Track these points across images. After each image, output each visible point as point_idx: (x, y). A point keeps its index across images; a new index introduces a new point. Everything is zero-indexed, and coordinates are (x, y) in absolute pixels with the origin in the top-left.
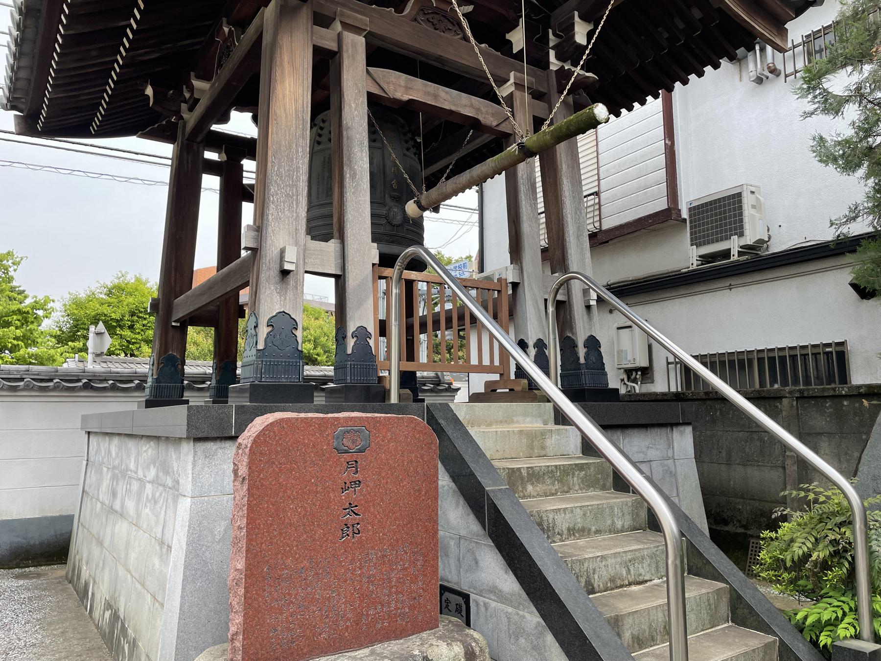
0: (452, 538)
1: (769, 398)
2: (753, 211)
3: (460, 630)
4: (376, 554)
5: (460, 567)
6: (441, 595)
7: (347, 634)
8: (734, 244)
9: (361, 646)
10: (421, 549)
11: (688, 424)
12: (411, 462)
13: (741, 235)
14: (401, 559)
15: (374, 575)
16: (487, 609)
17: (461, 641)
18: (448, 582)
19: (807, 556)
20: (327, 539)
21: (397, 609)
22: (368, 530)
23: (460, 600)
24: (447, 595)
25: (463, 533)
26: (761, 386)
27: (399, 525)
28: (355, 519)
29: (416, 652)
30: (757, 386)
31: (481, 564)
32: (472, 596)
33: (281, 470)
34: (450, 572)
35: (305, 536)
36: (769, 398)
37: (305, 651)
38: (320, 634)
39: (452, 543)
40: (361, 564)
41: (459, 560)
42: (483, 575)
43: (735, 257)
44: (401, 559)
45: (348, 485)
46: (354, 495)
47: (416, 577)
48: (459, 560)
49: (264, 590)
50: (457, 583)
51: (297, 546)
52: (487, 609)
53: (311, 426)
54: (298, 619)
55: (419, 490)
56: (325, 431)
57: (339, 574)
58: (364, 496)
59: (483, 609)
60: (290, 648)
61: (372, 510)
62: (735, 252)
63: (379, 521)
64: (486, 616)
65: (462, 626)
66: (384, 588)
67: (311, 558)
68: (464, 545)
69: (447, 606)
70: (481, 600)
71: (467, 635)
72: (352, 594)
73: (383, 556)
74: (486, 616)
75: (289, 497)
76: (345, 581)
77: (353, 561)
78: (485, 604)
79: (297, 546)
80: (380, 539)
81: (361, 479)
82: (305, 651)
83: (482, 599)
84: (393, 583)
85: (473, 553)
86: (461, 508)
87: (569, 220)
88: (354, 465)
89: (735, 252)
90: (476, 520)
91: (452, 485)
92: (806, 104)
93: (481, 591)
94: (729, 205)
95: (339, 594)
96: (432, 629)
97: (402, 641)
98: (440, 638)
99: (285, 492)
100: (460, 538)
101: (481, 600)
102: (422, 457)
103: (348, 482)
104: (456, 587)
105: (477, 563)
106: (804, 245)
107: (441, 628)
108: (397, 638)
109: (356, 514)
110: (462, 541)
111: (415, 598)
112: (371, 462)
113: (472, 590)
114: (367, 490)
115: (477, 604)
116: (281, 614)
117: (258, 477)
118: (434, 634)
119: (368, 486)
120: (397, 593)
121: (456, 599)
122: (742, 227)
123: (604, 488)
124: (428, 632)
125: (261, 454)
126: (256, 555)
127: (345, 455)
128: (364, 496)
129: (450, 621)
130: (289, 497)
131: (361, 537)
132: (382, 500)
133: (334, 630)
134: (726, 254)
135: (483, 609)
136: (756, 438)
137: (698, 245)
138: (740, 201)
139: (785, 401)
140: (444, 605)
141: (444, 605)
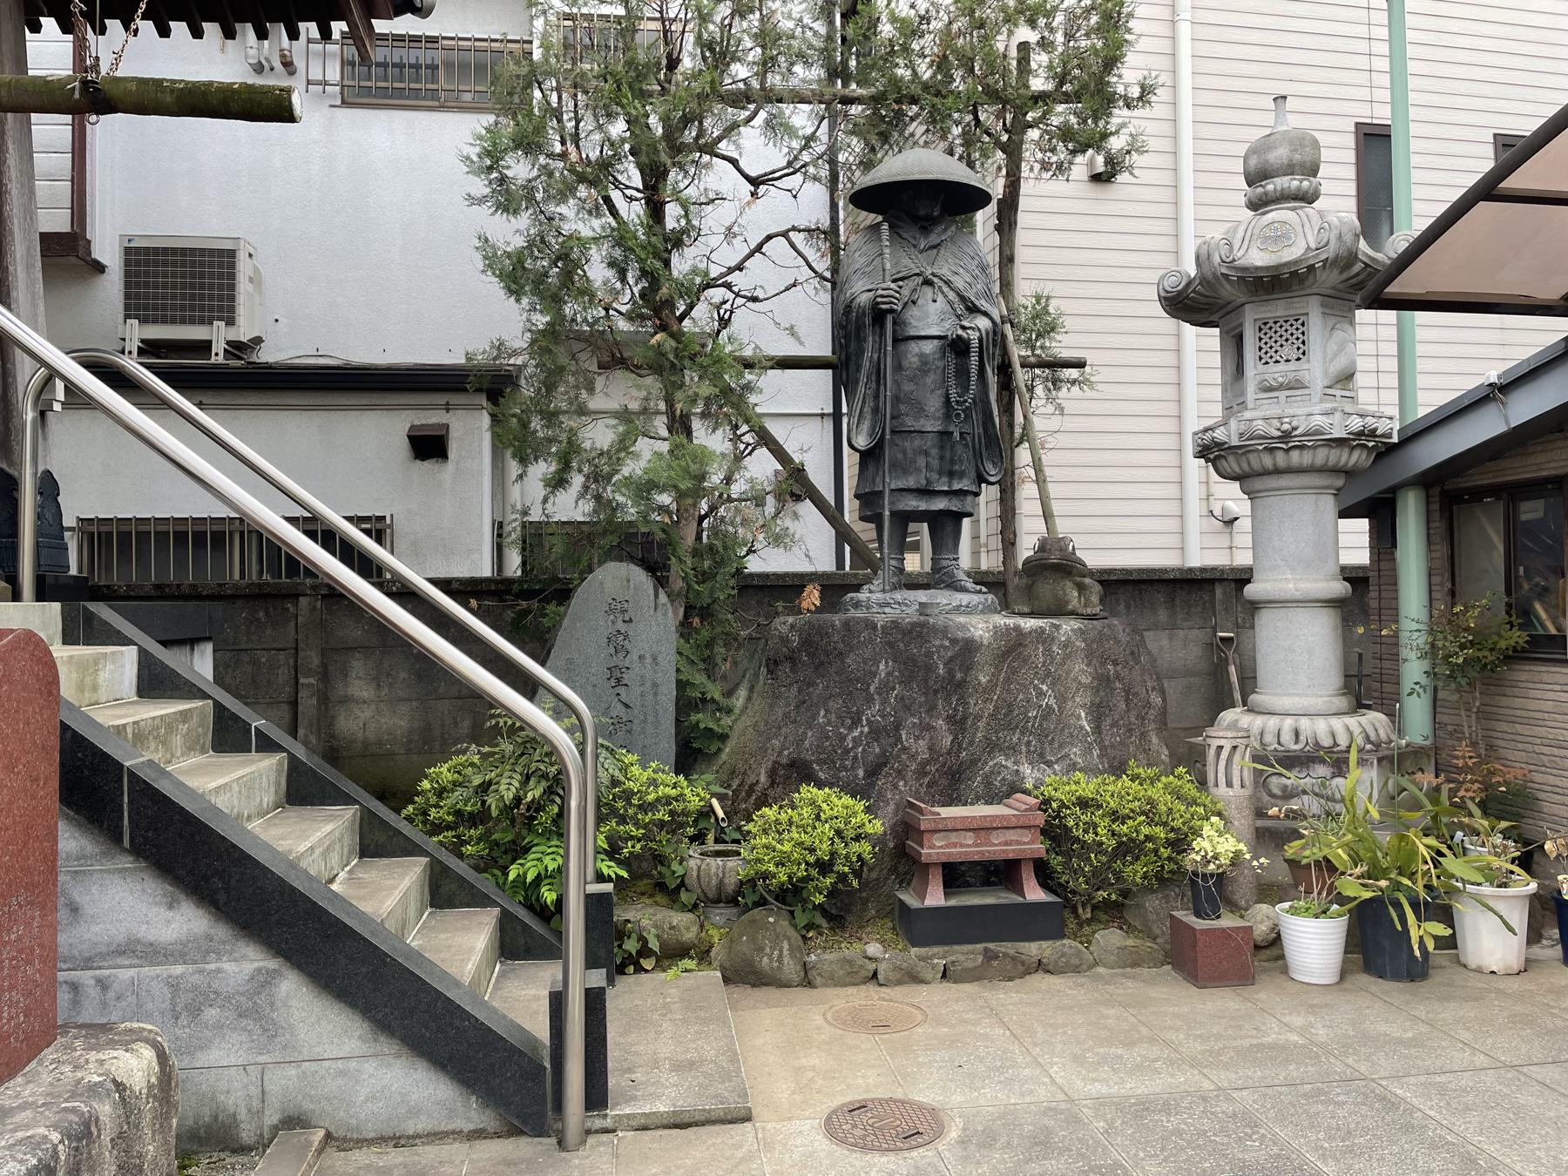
1: (276, 596)
2: (250, 287)
8: (219, 335)
11: (208, 639)
13: (231, 322)
19: (518, 800)
26: (242, 576)
30: (237, 576)
36: (276, 596)
42: (95, 929)
43: (218, 357)
62: (219, 347)
87: (16, 229)
89: (219, 347)
92: (480, 187)
94: (211, 265)
106: (297, 361)
122: (232, 309)
123: (203, 751)
134: (204, 347)
136: (246, 659)
137: (144, 321)
138: (232, 265)
139: (303, 601)
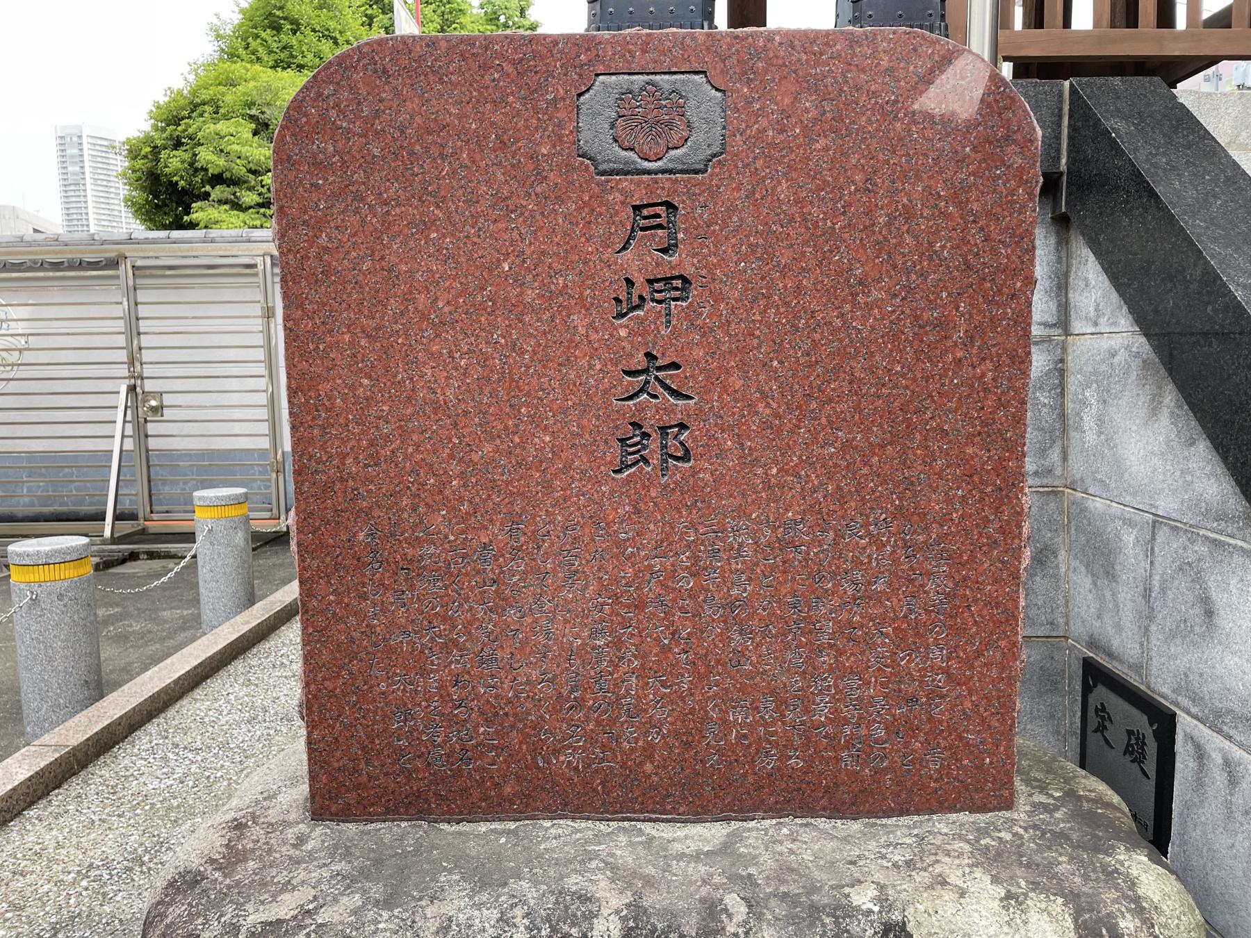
0: (1129, 522)
3: (1094, 833)
4: (754, 534)
5: (1151, 618)
6: (1086, 690)
7: (648, 767)
9: (700, 812)
10: (941, 538)
12: (909, 214)
14: (857, 562)
15: (747, 603)
16: (1233, 781)
17: (1072, 898)
18: (1110, 655)
20: (568, 466)
21: (838, 720)
22: (722, 453)
23: (1140, 722)
24: (1102, 694)
25: (1166, 506)
27: (847, 446)
28: (670, 410)
29: (864, 898)
31: (1225, 620)
32: (1185, 723)
33: (387, 225)
34: (1119, 627)
35: (488, 448)
37: (508, 790)
38: (557, 752)
39: (1129, 538)
40: (695, 559)
41: (1147, 594)
42: (1232, 661)
44: (857, 562)
45: (641, 287)
46: (660, 326)
47: (919, 630)
48: (1147, 594)
49: (364, 597)
50: (1137, 668)
51: (461, 475)
52: (1233, 781)
53: (485, 67)
54: (478, 697)
55: (943, 325)
56: (539, 88)
57: (615, 580)
58: (705, 331)
59: (1219, 777)
60: (458, 774)
61: (736, 382)
63: (766, 425)
64: (1228, 805)
65: (1110, 824)
66: (787, 646)
67: (514, 519)
68: (1168, 547)
69: (1101, 729)
70: (1214, 743)
71: (1111, 874)
72: (666, 650)
73: (785, 545)
74: (1228, 805)
75: (424, 317)
76: (639, 606)
77: (664, 546)
78: (1227, 763)
79: (461, 475)
80: (767, 486)
81: (689, 271)
82: (508, 790)
83: (1218, 740)
84: (825, 639)
85: (1198, 579)
86: (1165, 419)
88: (655, 216)
90: (1216, 459)
91: (1140, 343)
93: (1218, 714)
95: (618, 643)
96: (983, 809)
97: (855, 826)
98: (994, 860)
99: (407, 299)
100: (1158, 522)
101: (1214, 743)
102: (959, 195)
103: (639, 280)
104: (1133, 679)
105: (1209, 614)
107: (1020, 814)
108: (837, 811)
109: (676, 394)
110: (1163, 534)
111: (913, 699)
112: (732, 209)
113: (1185, 702)
114: (716, 313)
115: (1200, 754)
116: (424, 673)
117: (311, 242)
118: (983, 832)
119: (718, 298)
120: (839, 671)
121: (1126, 716)
124: (964, 817)
125: (317, 164)
126: (327, 487)
127: (626, 183)
128: (705, 331)
129: (1071, 795)
130: (424, 317)
131: (694, 472)
132: (778, 350)
133: (604, 747)
135: (1219, 777)
140: (1093, 721)
141: (1093, 721)
